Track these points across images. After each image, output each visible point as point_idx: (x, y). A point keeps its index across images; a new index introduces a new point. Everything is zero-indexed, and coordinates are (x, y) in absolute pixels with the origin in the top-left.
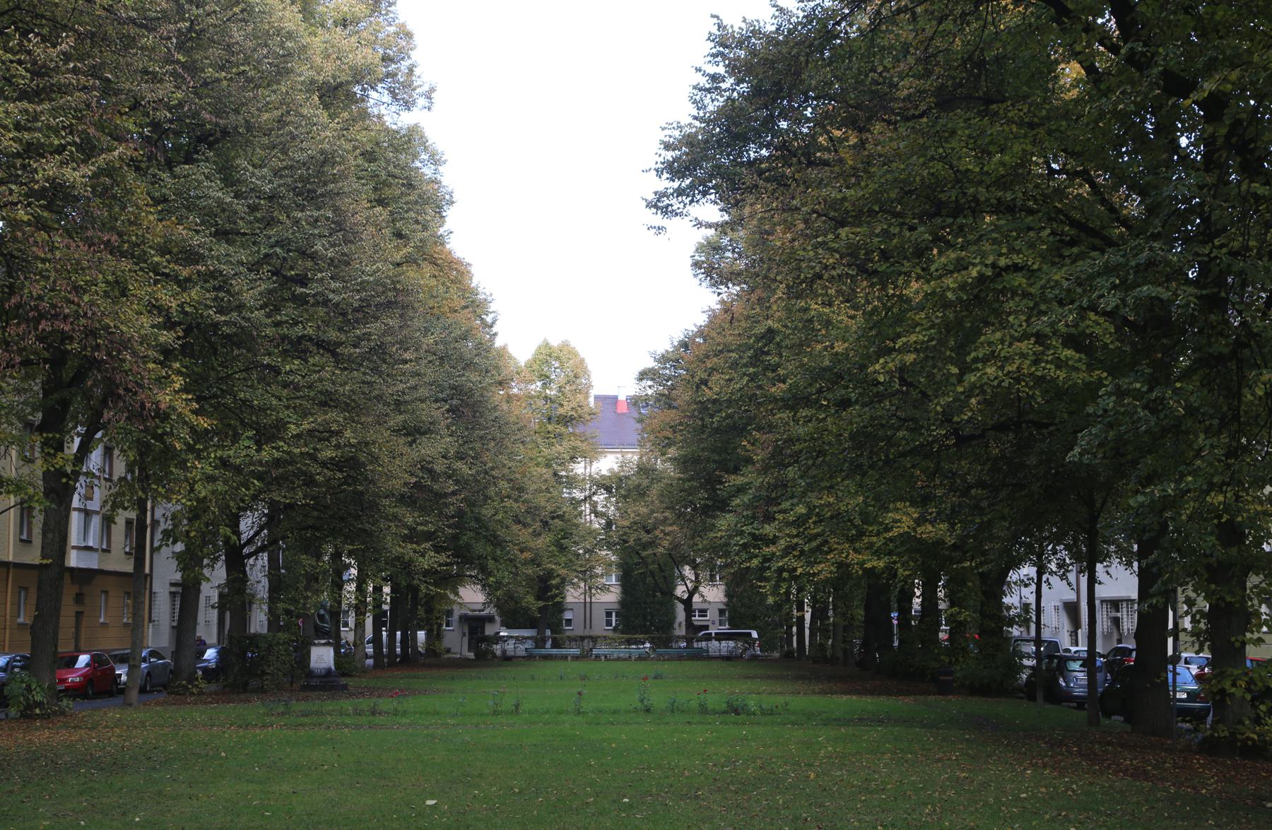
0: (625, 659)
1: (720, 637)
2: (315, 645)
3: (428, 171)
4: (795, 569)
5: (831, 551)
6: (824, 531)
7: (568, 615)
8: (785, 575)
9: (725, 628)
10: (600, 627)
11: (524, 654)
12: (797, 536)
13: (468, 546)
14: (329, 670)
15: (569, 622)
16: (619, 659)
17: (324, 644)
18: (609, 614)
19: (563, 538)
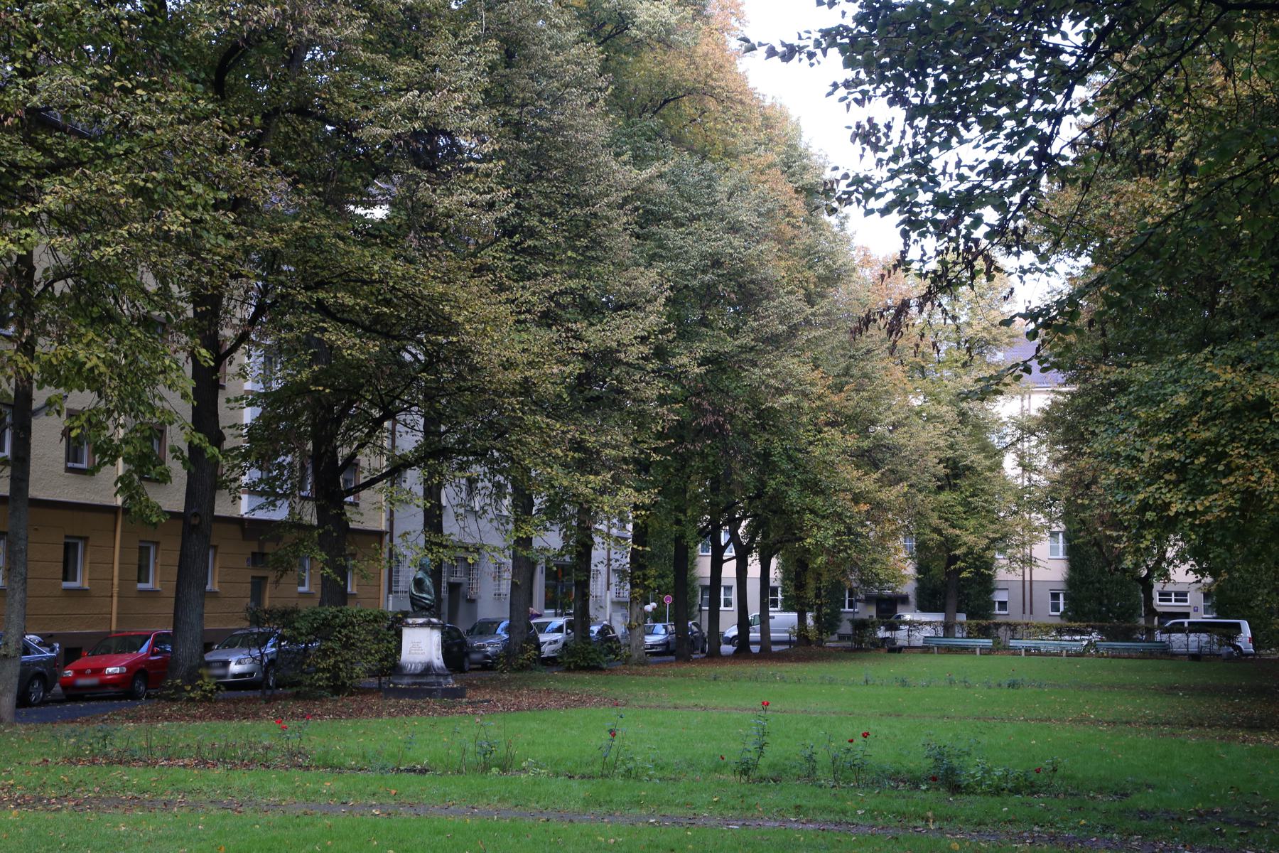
0: (1054, 655)
1: (1197, 628)
2: (408, 625)
3: (881, 110)
4: (1167, 506)
5: (1229, 471)
6: (1219, 435)
7: (999, 596)
8: (1150, 515)
9: (1209, 618)
10: (1045, 612)
11: (920, 643)
12: (1170, 447)
13: (779, 496)
14: (428, 669)
15: (1003, 605)
16: (1048, 654)
17: (421, 625)
18: (1055, 596)
19: (973, 496)
